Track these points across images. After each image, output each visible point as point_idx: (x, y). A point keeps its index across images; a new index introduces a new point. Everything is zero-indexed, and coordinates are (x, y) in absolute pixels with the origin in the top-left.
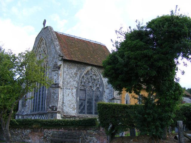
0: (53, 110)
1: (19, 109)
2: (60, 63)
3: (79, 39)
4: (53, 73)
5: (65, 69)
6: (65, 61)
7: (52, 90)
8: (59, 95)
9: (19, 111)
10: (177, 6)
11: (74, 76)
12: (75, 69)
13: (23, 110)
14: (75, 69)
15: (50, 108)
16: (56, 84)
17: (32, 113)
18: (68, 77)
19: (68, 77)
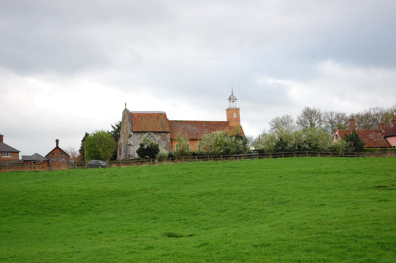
0: (129, 156)
1: (118, 156)
2: (132, 133)
3: (135, 113)
4: (128, 139)
5: (135, 136)
6: (134, 132)
7: (128, 147)
8: (132, 149)
9: (118, 158)
10: (259, 135)
11: (140, 138)
12: (140, 135)
13: (120, 157)
14: (140, 135)
15: (128, 155)
16: (130, 144)
17: (124, 158)
18: (136, 139)
19: (136, 139)
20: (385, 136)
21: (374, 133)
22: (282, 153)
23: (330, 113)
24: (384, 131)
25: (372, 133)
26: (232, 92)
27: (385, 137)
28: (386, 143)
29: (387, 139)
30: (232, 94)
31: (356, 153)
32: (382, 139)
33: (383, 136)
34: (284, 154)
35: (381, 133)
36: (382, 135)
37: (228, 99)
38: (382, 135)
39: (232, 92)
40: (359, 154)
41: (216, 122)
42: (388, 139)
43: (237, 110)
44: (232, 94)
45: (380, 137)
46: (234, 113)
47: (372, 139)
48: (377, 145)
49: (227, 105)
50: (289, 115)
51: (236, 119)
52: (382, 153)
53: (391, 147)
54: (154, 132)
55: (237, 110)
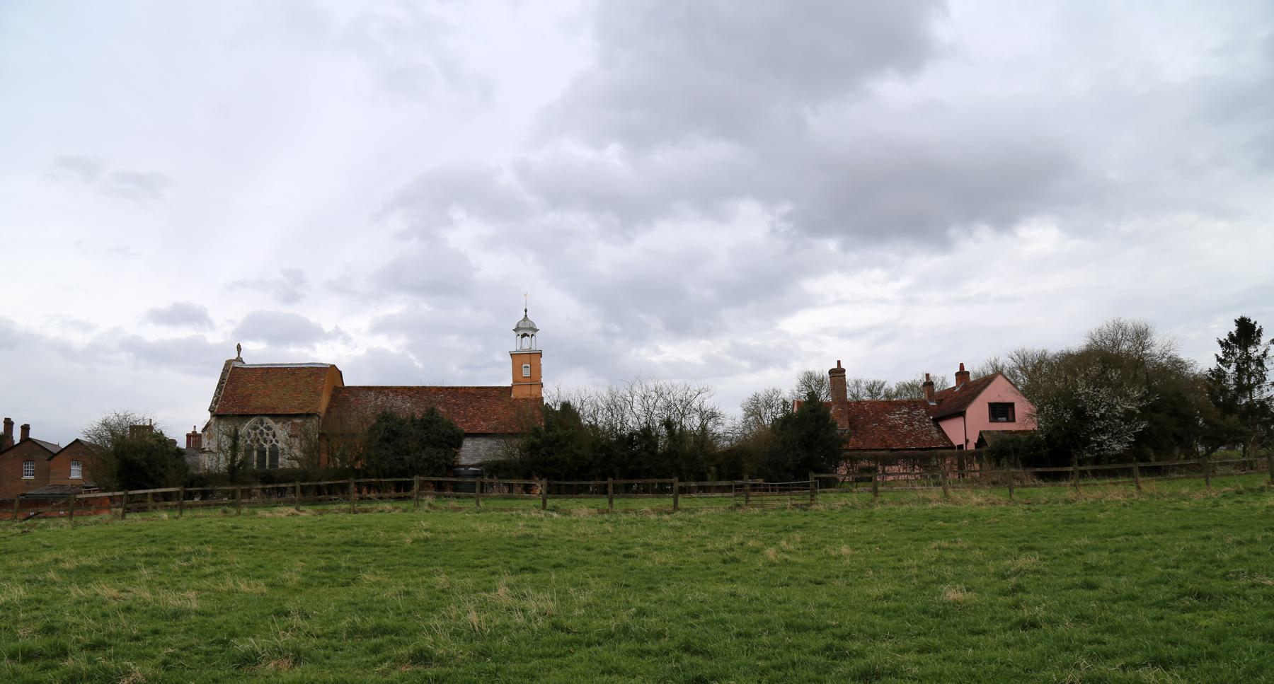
20: (936, 416)
21: (905, 410)
22: (474, 484)
23: (854, 383)
24: (935, 404)
25: (900, 410)
26: (526, 311)
27: (936, 421)
28: (936, 436)
29: (944, 425)
30: (526, 316)
31: (682, 484)
32: (929, 424)
33: (931, 417)
34: (1141, 469)
35: (926, 409)
36: (928, 416)
37: (515, 330)
38: (928, 416)
39: (526, 311)
40: (785, 485)
41: (478, 388)
42: (944, 425)
43: (536, 356)
44: (526, 316)
45: (921, 418)
46: (524, 365)
47: (896, 426)
48: (911, 443)
49: (514, 344)
50: (777, 389)
51: (529, 380)
52: (186, 492)
53: (953, 447)
54: (274, 416)
55: (536, 356)
